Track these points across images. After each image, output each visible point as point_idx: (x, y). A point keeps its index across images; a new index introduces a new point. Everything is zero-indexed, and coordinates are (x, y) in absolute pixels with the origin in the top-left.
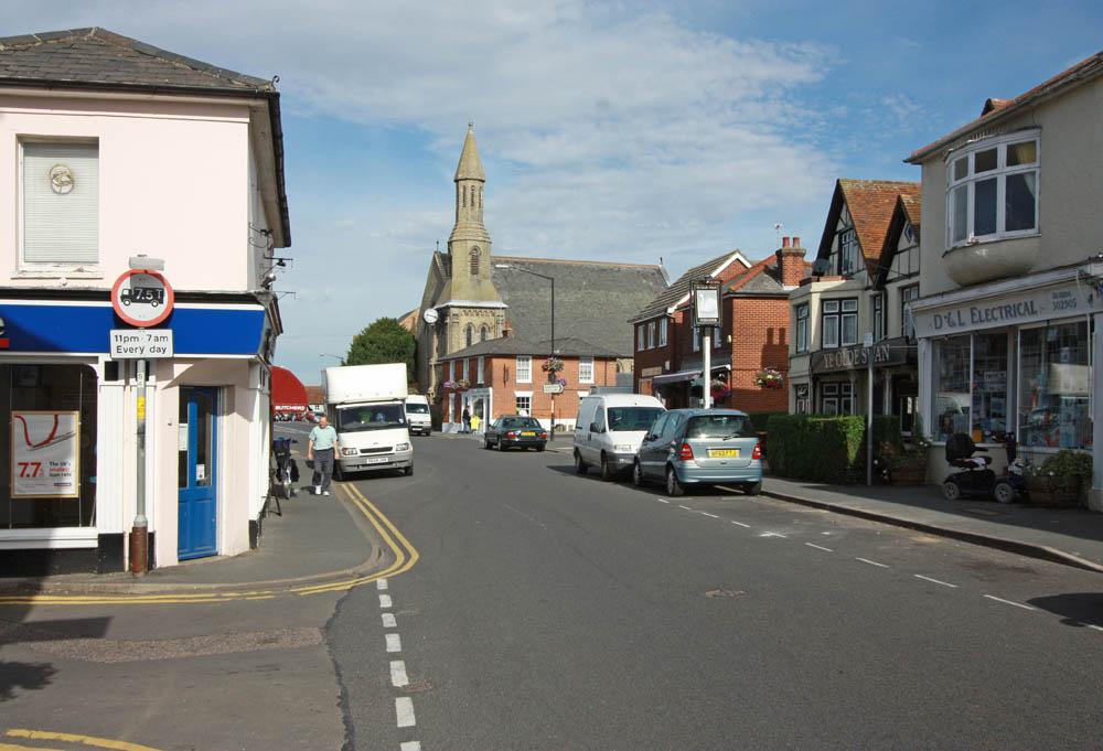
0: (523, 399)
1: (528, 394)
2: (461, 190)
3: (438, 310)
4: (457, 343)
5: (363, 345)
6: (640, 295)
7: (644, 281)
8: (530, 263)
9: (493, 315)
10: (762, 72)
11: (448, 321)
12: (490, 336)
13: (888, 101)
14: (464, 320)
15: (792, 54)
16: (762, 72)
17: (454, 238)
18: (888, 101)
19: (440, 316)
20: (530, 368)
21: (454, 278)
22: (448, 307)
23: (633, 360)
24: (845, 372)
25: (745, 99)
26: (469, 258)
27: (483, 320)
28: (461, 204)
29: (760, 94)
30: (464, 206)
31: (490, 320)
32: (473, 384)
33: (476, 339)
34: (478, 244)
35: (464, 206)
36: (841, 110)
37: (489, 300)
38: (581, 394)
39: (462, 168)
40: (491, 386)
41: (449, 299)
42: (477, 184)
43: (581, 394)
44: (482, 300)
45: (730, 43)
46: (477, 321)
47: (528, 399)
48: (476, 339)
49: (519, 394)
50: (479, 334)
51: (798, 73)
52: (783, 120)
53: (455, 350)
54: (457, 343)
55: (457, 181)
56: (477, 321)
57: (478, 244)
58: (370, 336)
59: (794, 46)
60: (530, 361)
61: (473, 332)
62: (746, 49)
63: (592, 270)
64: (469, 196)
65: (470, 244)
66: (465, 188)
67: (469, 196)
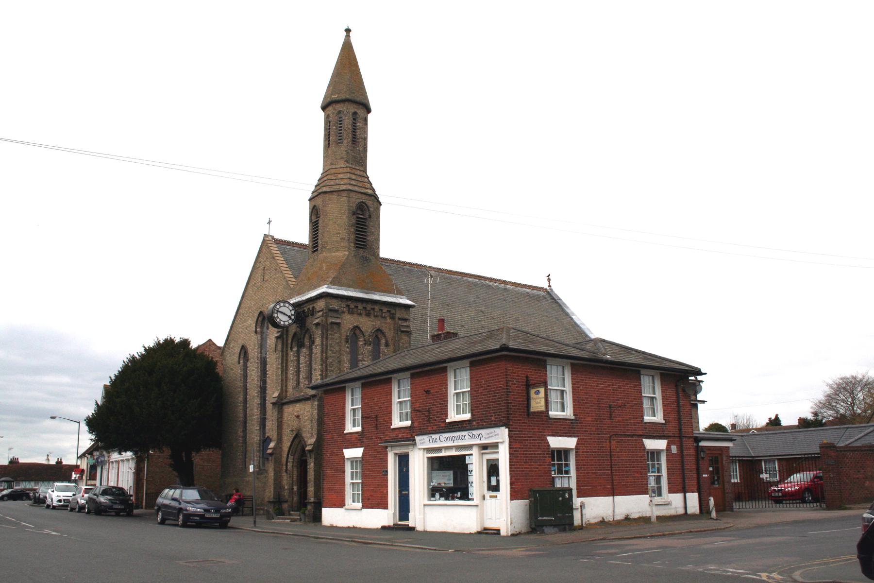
9: (393, 317)
43: (556, 442)
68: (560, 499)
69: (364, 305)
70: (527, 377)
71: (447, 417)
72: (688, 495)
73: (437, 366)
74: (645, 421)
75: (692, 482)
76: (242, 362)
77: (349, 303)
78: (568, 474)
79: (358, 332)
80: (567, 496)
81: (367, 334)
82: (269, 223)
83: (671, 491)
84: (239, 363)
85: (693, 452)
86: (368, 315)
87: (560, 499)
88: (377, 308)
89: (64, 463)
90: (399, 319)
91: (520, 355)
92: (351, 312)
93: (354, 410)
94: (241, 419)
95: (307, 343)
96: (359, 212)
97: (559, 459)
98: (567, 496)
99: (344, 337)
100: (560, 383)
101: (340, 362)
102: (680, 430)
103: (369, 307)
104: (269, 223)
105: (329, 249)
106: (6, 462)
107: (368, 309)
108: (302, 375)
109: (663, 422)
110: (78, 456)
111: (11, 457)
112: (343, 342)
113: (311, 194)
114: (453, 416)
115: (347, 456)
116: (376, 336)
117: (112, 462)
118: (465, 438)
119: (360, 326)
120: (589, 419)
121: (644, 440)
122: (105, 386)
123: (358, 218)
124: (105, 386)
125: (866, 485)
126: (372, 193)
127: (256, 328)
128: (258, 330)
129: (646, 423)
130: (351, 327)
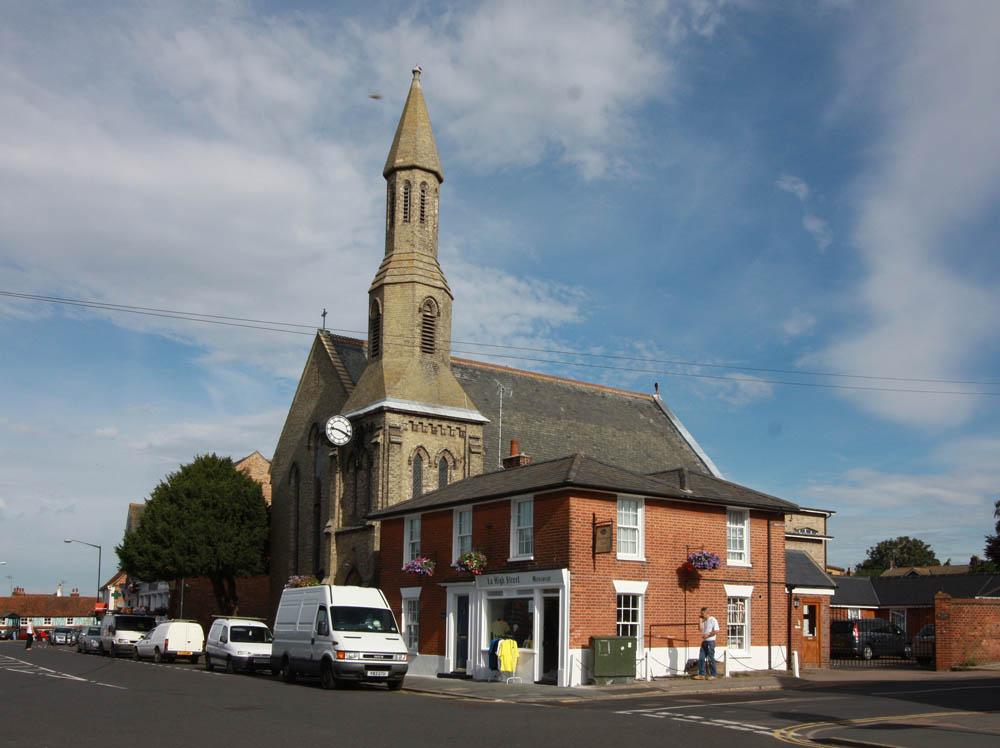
0: (627, 597)
1: (638, 587)
2: (401, 190)
3: (353, 421)
4: (398, 487)
5: (172, 501)
6: (644, 436)
7: (642, 417)
8: (475, 370)
9: (462, 435)
10: (533, 309)
11: (380, 439)
12: (456, 476)
13: (639, 345)
14: (411, 440)
15: (564, 296)
16: (533, 309)
17: (388, 280)
18: (639, 345)
19: (355, 431)
20: (641, 526)
21: (386, 359)
22: (381, 411)
23: (771, 522)
24: (872, 579)
25: (518, 334)
26: (419, 319)
27: (446, 442)
28: (400, 215)
29: (530, 330)
30: (407, 219)
31: (457, 445)
32: (497, 562)
33: (385, 506)
34: (435, 293)
35: (407, 219)
36: (597, 351)
37: (453, 404)
38: (732, 590)
39: (402, 147)
40: (567, 566)
41: (382, 396)
42: (431, 180)
43: (732, 590)
44: (442, 402)
45: (510, 281)
46: (434, 444)
47: (635, 598)
48: (431, 485)
49: (623, 587)
50: (436, 471)
51: (563, 314)
52: (546, 356)
53: (392, 502)
54: (398, 487)
55: (390, 173)
56: (434, 444)
57: (435, 293)
58: (187, 484)
59: (566, 288)
60: (641, 511)
61: (425, 465)
62: (522, 286)
63: (568, 391)
64: (416, 200)
65: (422, 292)
66: (408, 185)
67: (416, 200)
68: (623, 648)
69: (430, 421)
70: (594, 514)
71: (508, 556)
72: (772, 647)
73: (391, 518)
74: (619, 558)
75: (780, 632)
76: (293, 481)
77: (413, 419)
78: (934, 668)
79: (422, 452)
80: (630, 645)
81: (432, 456)
82: (324, 315)
83: (753, 643)
84: (290, 483)
85: (783, 600)
86: (434, 432)
87: (623, 648)
88: (445, 424)
89: (81, 596)
90: (470, 438)
91: (495, 501)
92: (414, 430)
93: (413, 544)
94: (292, 549)
95: (365, 465)
96: (427, 309)
97: (627, 604)
98: (630, 645)
99: (406, 459)
100: (631, 519)
101: (400, 487)
102: (769, 575)
103: (436, 423)
104: (324, 315)
105: (391, 354)
106: (8, 594)
107: (434, 425)
108: (360, 501)
109: (750, 565)
110: (101, 586)
111: (15, 586)
112: (405, 463)
113: (371, 285)
114: (515, 554)
115: (404, 596)
116: (444, 458)
117: (142, 597)
118: (525, 580)
119: (425, 446)
120: (662, 561)
121: (725, 586)
122: (133, 508)
123: (425, 316)
124: (133, 508)
125: (983, 643)
126: (443, 286)
127: (309, 443)
128: (311, 445)
129: (729, 567)
130: (415, 446)
